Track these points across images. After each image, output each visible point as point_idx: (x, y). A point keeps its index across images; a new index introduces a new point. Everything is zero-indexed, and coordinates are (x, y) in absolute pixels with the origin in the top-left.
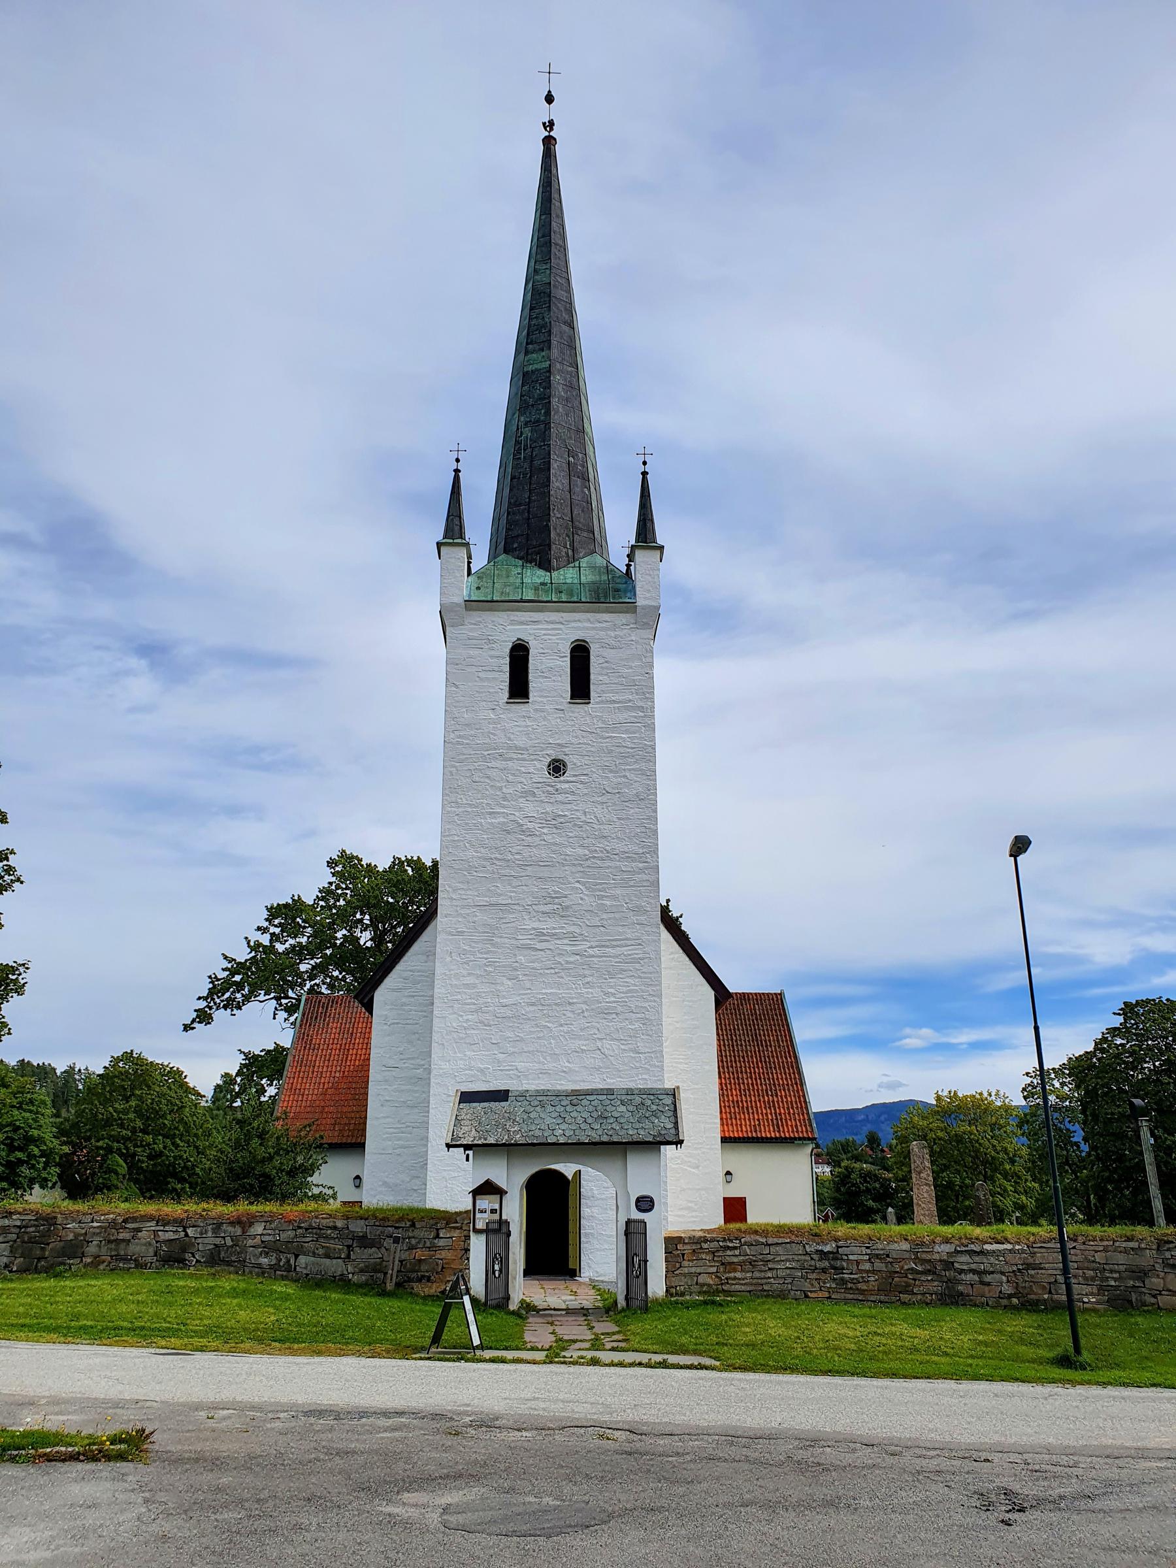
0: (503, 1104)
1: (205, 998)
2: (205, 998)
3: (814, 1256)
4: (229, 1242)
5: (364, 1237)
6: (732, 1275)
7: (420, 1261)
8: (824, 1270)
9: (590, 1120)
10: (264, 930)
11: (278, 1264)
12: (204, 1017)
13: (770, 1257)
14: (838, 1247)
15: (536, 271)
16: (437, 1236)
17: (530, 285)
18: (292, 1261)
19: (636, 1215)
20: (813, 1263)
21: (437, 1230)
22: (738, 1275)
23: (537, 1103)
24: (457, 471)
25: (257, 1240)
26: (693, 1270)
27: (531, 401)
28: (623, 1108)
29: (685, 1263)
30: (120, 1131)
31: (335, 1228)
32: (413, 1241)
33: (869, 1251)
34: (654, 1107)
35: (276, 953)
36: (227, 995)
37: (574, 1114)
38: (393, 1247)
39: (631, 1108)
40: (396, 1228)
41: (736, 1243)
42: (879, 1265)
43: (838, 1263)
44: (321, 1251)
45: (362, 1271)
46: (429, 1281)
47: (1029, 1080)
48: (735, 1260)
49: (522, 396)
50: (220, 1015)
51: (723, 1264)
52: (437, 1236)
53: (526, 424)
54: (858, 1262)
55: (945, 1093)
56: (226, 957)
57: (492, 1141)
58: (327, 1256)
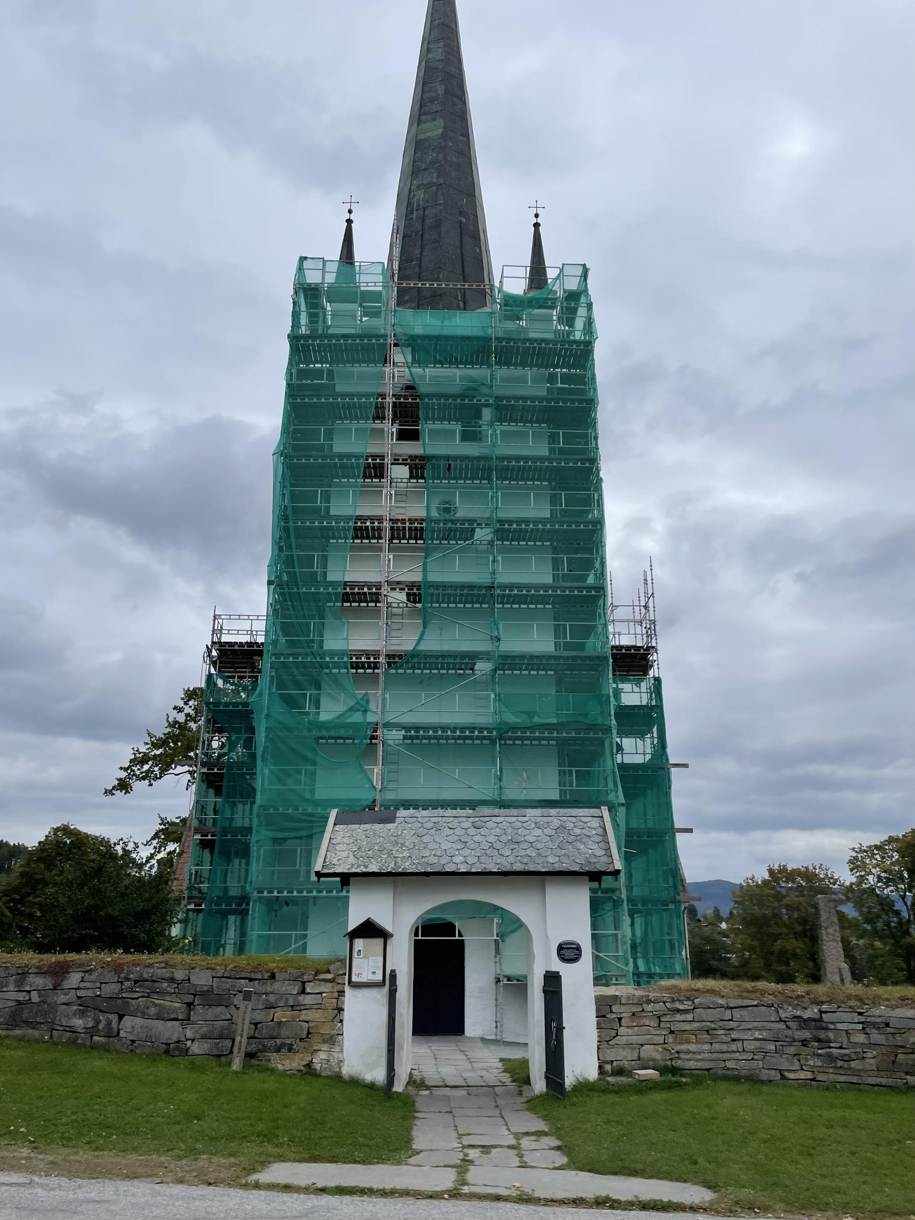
0: (389, 826)
1: (126, 769)
2: (126, 769)
3: (790, 1024)
4: (35, 997)
5: (210, 991)
6: (684, 1047)
7: (280, 1023)
8: (804, 1043)
9: (498, 845)
10: (180, 710)
11: (95, 1027)
12: (123, 786)
13: (732, 1024)
14: (821, 1012)
15: (428, 50)
16: (303, 991)
17: (424, 63)
18: (114, 1025)
19: (557, 965)
20: (790, 1033)
21: (304, 983)
22: (692, 1047)
23: (430, 825)
24: (349, 221)
25: (72, 996)
26: (634, 1039)
27: (424, 166)
28: (538, 832)
29: (622, 1030)
30: (68, 897)
31: (172, 980)
32: (272, 998)
33: (862, 1019)
34: (578, 831)
35: (190, 729)
36: (146, 767)
37: (478, 838)
38: (242, 1005)
39: (548, 832)
40: (251, 980)
41: (687, 1005)
42: (876, 1037)
43: (822, 1035)
44: (153, 1011)
45: (204, 1037)
46: (290, 1049)
47: (854, 854)
48: (687, 1027)
49: (414, 161)
50: (139, 786)
51: (672, 1032)
52: (303, 991)
53: (418, 187)
54: (847, 1032)
55: (776, 867)
56: (149, 734)
57: (373, 868)
58: (159, 1017)
